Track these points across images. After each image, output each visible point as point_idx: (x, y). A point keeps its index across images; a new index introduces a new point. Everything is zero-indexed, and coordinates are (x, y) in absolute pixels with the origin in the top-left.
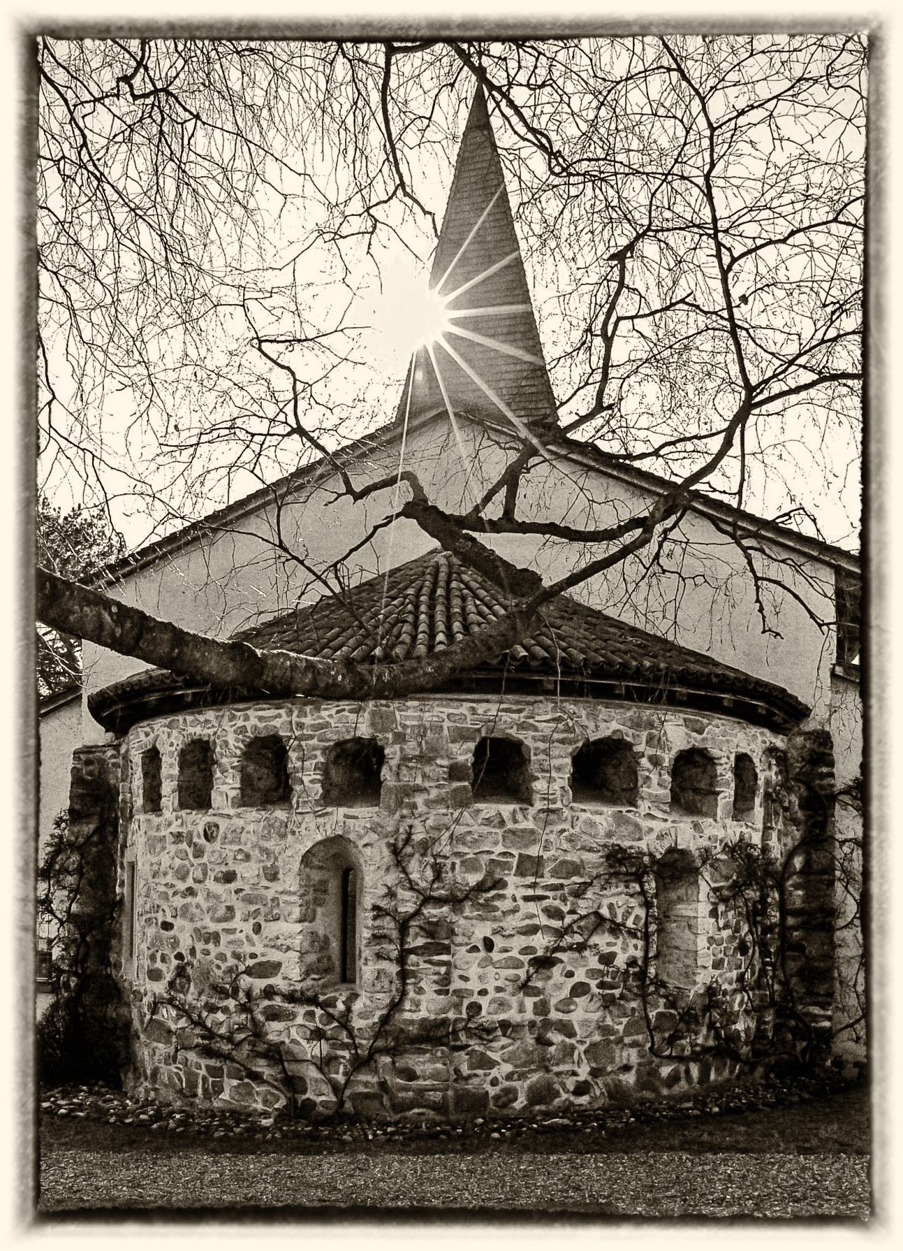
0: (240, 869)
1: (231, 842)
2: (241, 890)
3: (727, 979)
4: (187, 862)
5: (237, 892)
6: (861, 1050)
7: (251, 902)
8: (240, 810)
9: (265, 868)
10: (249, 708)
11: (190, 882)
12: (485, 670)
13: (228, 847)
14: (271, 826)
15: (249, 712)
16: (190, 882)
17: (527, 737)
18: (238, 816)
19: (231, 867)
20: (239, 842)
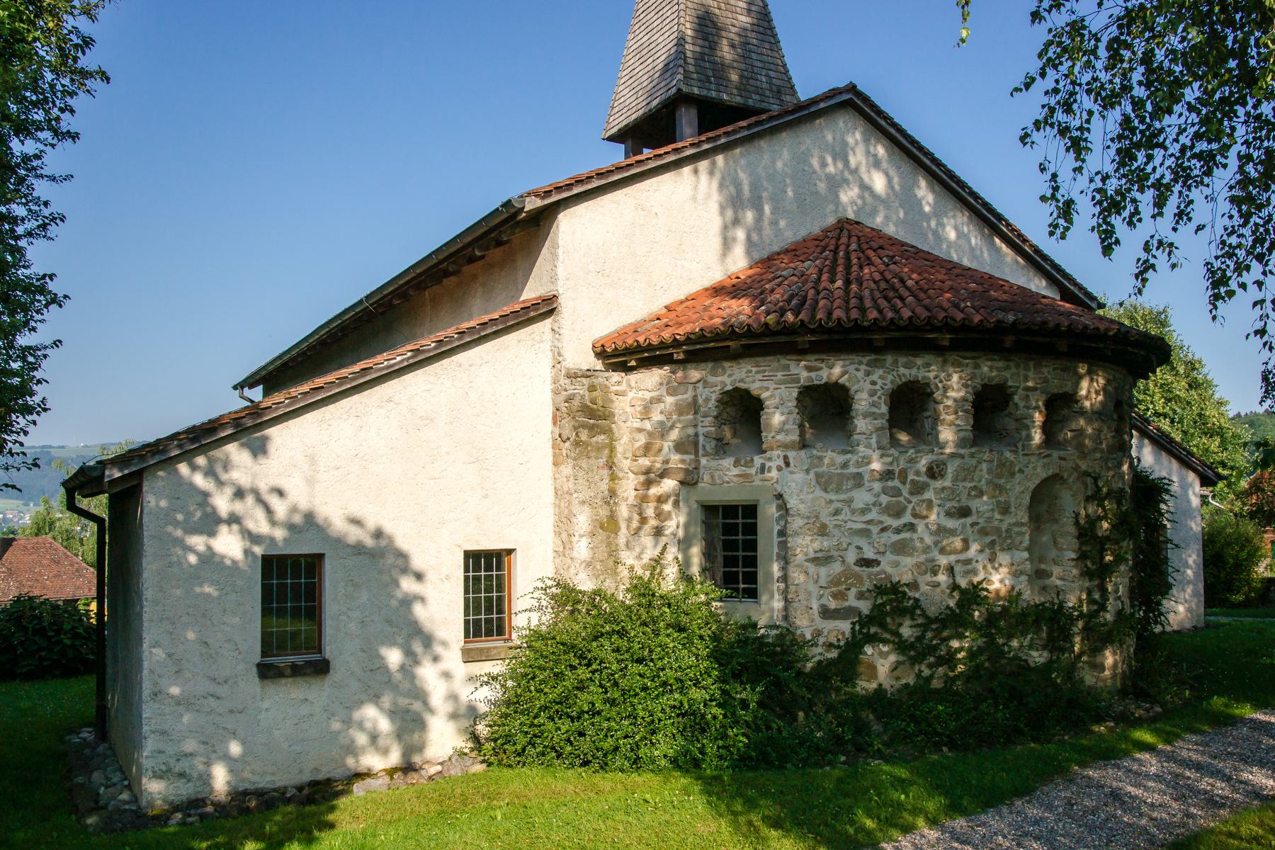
0: (975, 504)
1: (964, 480)
2: (977, 524)
3: (858, 689)
4: (901, 499)
5: (972, 525)
6: (276, 625)
7: (986, 534)
8: (973, 450)
9: (998, 503)
10: (978, 358)
11: (908, 518)
12: (767, 336)
13: (961, 484)
14: (1004, 465)
15: (979, 361)
16: (908, 518)
17: (764, 395)
18: (972, 456)
19: (964, 502)
20: (972, 480)
